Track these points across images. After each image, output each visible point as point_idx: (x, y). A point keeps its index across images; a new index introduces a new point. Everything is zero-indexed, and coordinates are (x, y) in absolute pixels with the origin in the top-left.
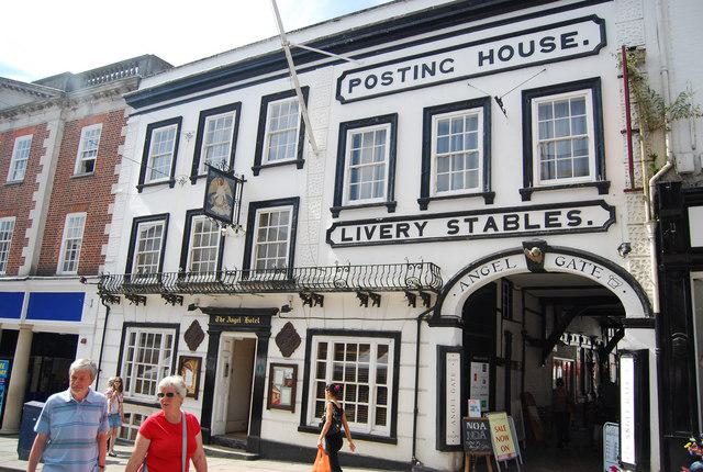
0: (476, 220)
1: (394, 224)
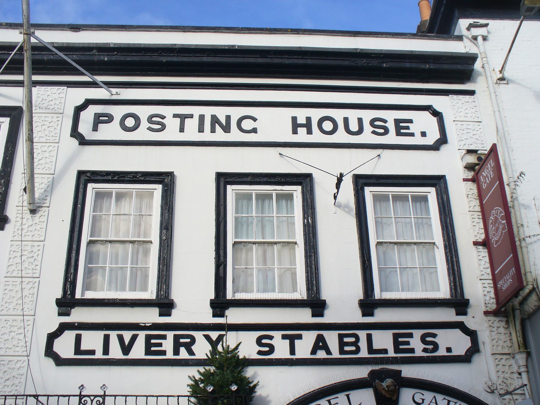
0: (300, 337)
1: (170, 335)
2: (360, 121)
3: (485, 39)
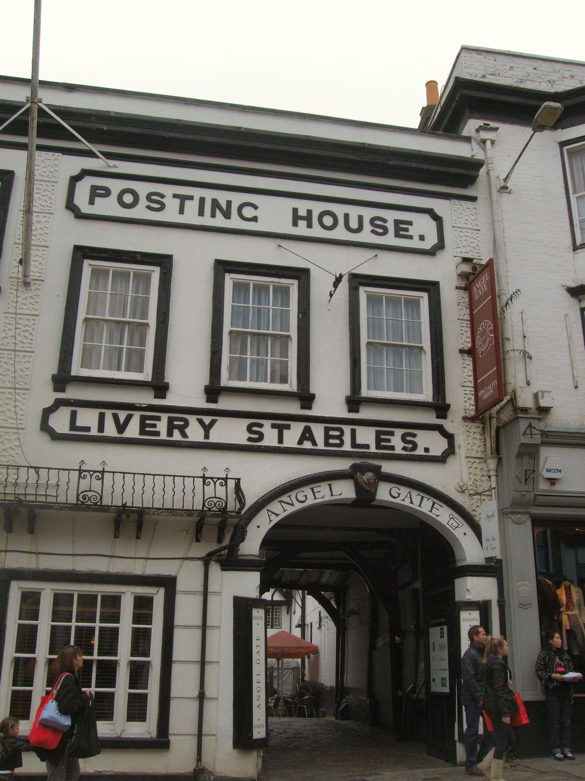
0: (288, 427)
1: (165, 417)
2: (360, 218)
3: (493, 142)
